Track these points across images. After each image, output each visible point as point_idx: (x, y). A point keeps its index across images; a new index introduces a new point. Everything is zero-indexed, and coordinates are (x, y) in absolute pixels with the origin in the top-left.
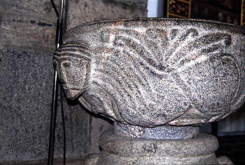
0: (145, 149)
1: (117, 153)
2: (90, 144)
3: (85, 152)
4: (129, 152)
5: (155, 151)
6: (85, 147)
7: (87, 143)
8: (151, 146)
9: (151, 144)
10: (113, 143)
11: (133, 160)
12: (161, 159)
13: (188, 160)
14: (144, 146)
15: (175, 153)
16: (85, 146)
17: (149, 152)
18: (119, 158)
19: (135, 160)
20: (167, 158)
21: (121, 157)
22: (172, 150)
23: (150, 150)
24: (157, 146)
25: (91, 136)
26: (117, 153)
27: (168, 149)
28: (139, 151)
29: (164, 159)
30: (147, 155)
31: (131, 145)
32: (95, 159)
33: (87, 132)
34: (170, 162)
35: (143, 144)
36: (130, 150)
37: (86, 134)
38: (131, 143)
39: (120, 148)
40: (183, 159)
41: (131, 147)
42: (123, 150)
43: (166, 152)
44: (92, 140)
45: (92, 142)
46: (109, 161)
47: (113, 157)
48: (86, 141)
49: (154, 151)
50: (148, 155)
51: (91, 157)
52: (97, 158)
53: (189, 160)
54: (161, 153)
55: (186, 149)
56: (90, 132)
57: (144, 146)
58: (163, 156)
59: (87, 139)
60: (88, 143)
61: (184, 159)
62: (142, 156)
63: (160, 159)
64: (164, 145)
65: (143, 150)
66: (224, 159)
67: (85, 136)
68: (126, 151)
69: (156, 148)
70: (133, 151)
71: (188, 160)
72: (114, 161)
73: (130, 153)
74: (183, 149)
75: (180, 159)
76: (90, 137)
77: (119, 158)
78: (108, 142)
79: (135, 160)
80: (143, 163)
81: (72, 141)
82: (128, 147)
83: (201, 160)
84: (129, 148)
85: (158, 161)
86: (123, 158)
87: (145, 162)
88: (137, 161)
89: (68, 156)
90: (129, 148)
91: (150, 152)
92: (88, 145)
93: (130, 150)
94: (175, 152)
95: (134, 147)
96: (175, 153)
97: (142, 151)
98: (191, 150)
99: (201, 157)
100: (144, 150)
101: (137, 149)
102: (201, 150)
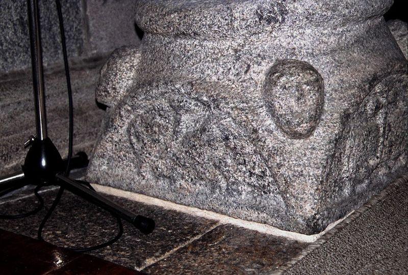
0: (261, 18)
1: (195, 34)
2: (89, 35)
3: (80, 53)
4: (226, 27)
5: (284, 19)
6: (79, 41)
7: (82, 33)
8: (274, 10)
9: (272, 5)
10: (182, 14)
11: (235, 45)
12: (294, 35)
13: (347, 30)
14: (259, 11)
15: (326, 19)
16: (77, 40)
17: (269, 23)
18: (201, 46)
19: (239, 45)
20: (308, 31)
21: (205, 43)
22: (320, 12)
23: (273, 18)
24: (287, 8)
25: (87, 15)
26: (195, 34)
27: (311, 11)
28: (248, 24)
29: (302, 34)
30: (267, 29)
31: (229, 11)
32: (134, 57)
33: (78, 8)
34: (315, 39)
35: (255, 7)
36: (228, 25)
37: (77, 13)
38: (228, 8)
39: (204, 23)
40: (338, 29)
41: (230, 17)
42: (210, 27)
43: (307, 18)
44: (91, 25)
45: (92, 29)
46: (175, 55)
47: (183, 46)
48: (79, 27)
49: (280, 19)
50: (269, 28)
51: (123, 54)
52: (138, 55)
53: (350, 31)
54: (295, 22)
55: (347, 8)
56: (85, 10)
57: (259, 11)
58: (301, 27)
59: (79, 23)
60: (84, 31)
61: (341, 30)
62: (255, 34)
63: (293, 36)
64: (303, 3)
65: (257, 19)
66: (398, 25)
67: (75, 17)
68: (219, 28)
69: (283, 12)
70: (236, 24)
71: (347, 30)
72: (189, 54)
73: (227, 31)
74: (340, 8)
75: (334, 31)
76: (86, 19)
77: (201, 46)
78: (169, 14)
79: (239, 45)
80: (257, 47)
81: (50, 29)
82: (222, 18)
83: (370, 28)
84: (226, 20)
85: (289, 40)
86: (209, 44)
87: (262, 46)
88: (243, 46)
89: (49, 65)
90: (226, 20)
91: (272, 23)
92: (83, 36)
93: (228, 25)
94: (325, 15)
95: (237, 15)
96: (326, 19)
97: (256, 21)
98: (356, 8)
99: (369, 22)
100: (260, 20)
101: (243, 20)
102: (373, 6)
